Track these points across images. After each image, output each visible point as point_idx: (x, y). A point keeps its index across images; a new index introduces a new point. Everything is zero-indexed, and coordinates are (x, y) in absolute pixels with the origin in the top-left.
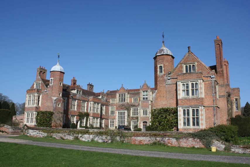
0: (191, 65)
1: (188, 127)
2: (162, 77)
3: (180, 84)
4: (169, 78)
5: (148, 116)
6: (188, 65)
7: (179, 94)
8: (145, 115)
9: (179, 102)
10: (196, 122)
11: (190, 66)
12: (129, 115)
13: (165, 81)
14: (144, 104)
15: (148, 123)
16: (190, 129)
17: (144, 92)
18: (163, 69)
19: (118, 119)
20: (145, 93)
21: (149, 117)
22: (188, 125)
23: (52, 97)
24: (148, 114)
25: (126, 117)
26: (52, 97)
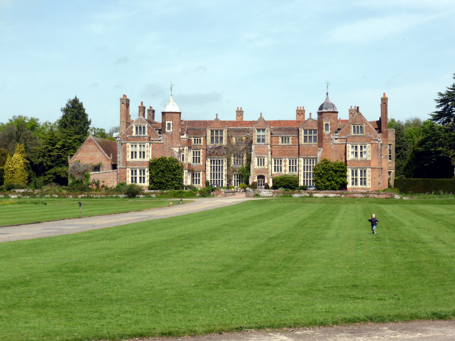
0: (359, 126)
1: (356, 186)
2: (329, 135)
3: (349, 146)
4: (337, 137)
5: (267, 167)
6: (356, 126)
7: (349, 155)
8: (261, 165)
9: (348, 163)
10: (364, 182)
11: (358, 127)
12: (228, 165)
13: (331, 139)
14: (259, 149)
15: (266, 178)
16: (358, 188)
17: (259, 130)
18: (330, 127)
19: (211, 171)
20: (261, 133)
21: (268, 168)
22: (356, 184)
23: (173, 148)
24: (266, 164)
25: (225, 168)
26: (173, 148)
